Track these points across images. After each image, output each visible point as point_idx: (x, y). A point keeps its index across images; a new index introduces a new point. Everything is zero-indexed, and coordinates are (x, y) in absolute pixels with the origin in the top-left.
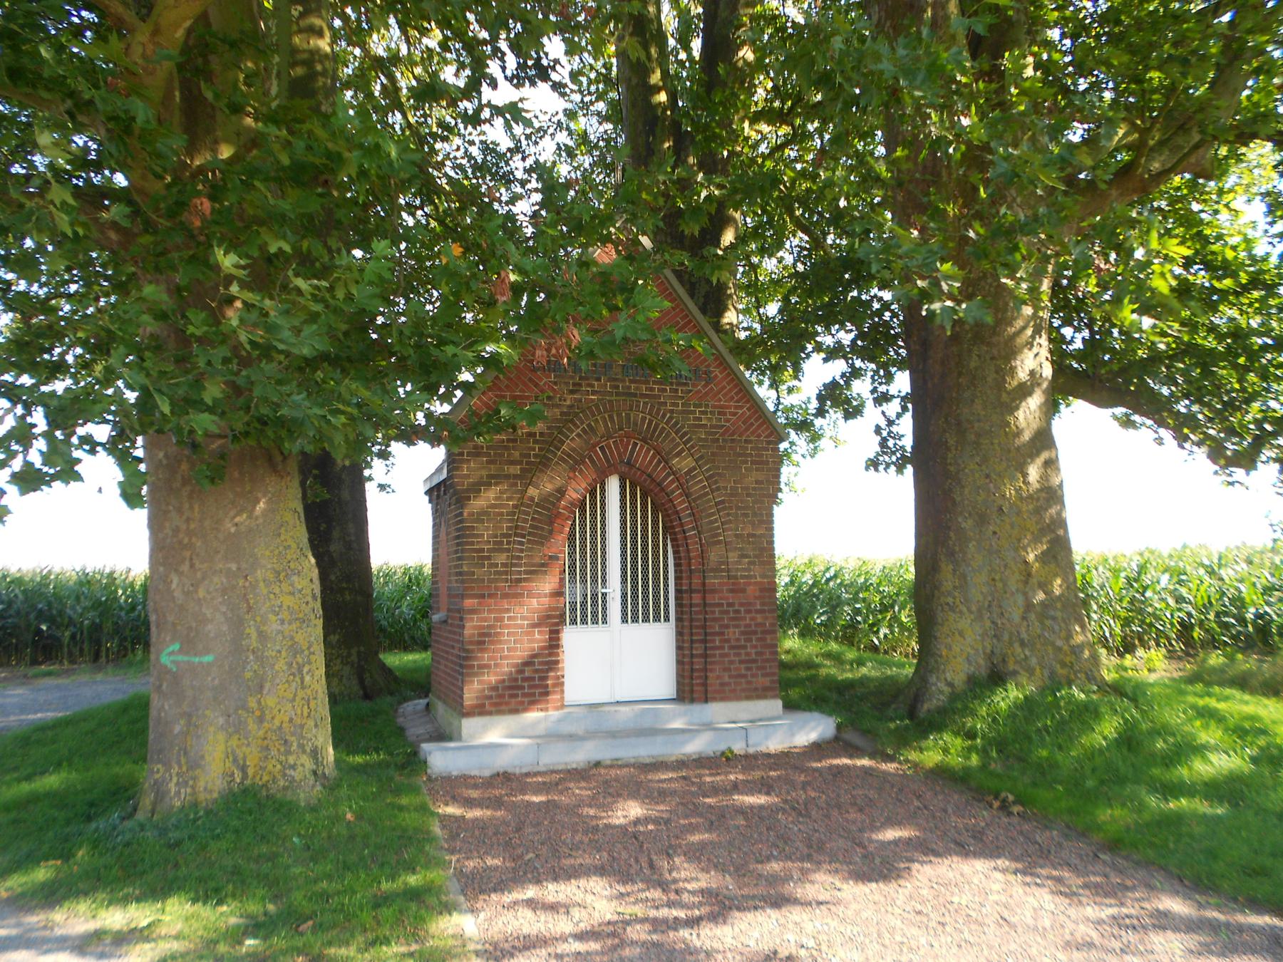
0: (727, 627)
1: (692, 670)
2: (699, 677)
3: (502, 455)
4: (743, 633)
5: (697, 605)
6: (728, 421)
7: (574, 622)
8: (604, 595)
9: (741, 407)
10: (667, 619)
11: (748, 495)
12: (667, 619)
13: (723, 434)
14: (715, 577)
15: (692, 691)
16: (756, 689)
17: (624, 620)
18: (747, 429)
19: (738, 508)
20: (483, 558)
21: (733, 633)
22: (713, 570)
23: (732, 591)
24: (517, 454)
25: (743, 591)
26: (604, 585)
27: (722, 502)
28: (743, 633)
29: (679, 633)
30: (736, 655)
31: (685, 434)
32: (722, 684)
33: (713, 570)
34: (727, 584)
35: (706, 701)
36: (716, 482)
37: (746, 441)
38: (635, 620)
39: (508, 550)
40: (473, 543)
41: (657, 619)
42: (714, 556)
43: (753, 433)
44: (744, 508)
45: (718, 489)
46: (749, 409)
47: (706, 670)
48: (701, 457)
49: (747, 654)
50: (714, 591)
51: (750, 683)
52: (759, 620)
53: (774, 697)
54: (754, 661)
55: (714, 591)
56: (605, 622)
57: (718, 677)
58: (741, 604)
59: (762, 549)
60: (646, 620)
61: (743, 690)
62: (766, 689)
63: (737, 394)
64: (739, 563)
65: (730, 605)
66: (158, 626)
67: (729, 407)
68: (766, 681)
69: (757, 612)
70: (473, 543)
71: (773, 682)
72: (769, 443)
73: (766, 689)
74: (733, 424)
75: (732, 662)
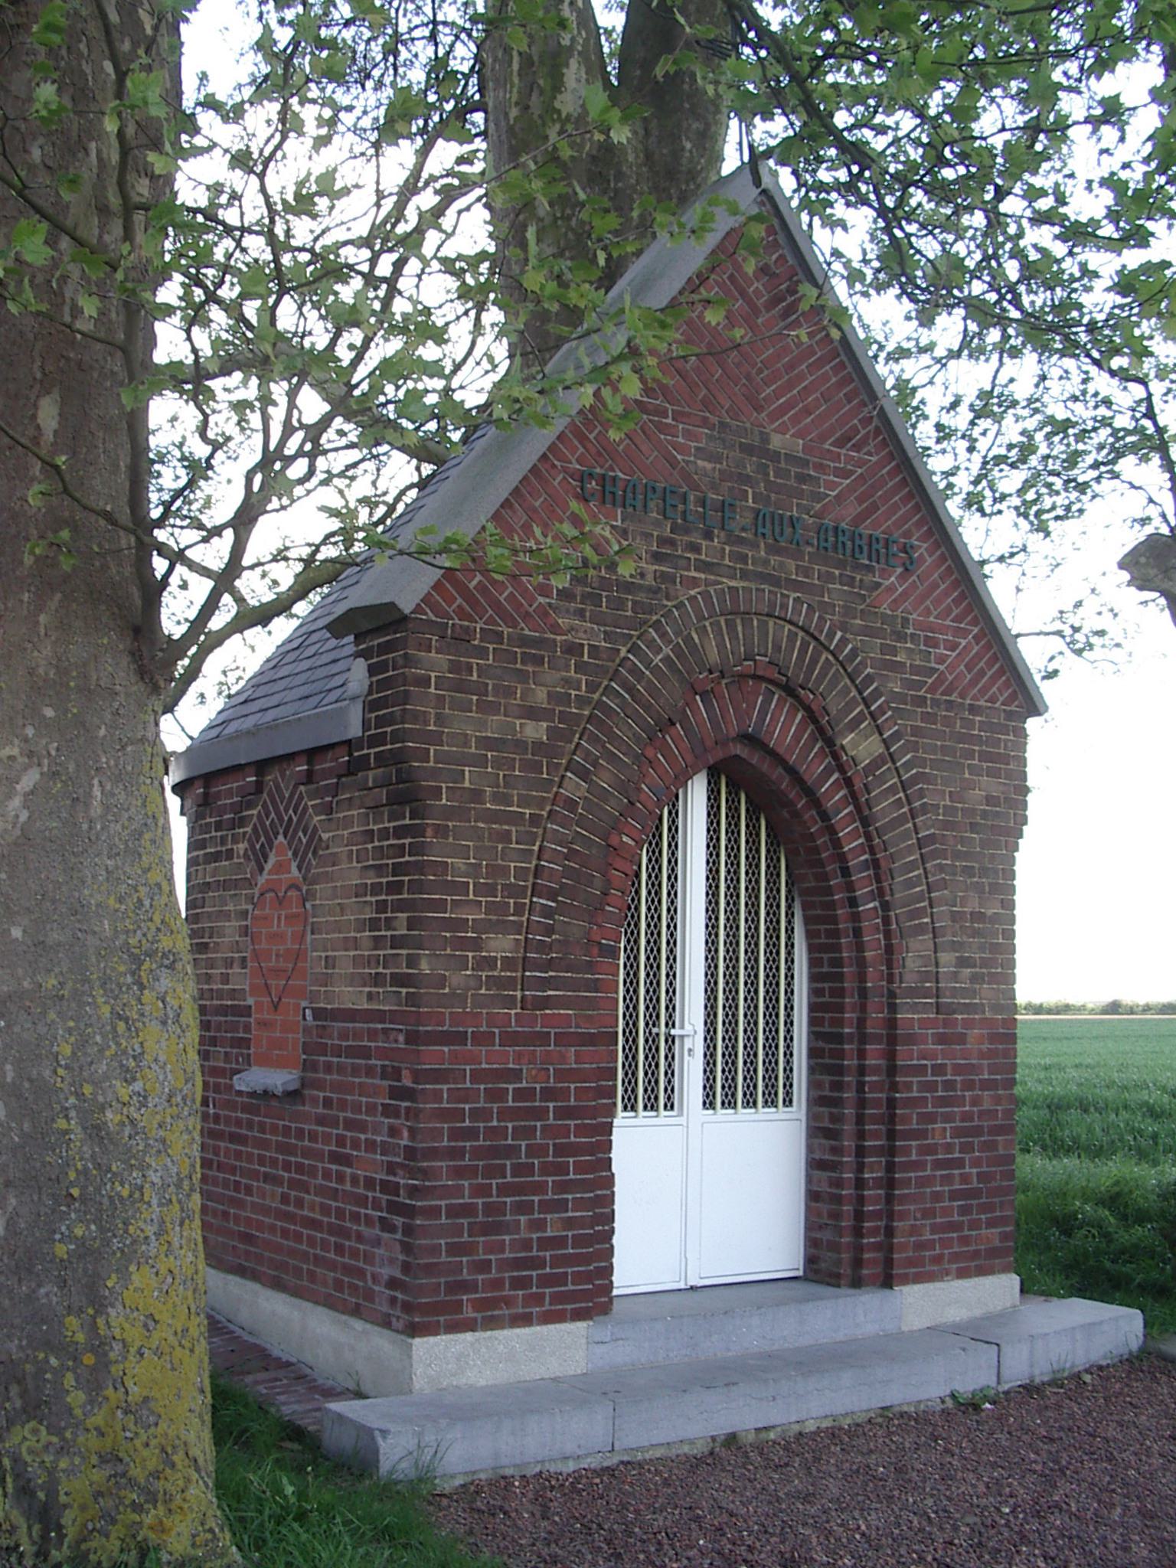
0: (931, 1118)
1: (859, 1216)
2: (875, 1231)
3: (510, 692)
4: (958, 1133)
5: (876, 1070)
6: (941, 660)
7: (630, 1106)
8: (671, 1040)
9: (964, 633)
10: (788, 1102)
11: (973, 827)
12: (788, 1102)
13: (932, 689)
14: (914, 1008)
15: (858, 1263)
16: (976, 1254)
17: (709, 1103)
18: (974, 682)
19: (957, 856)
20: (463, 944)
21: (942, 1133)
22: (913, 992)
23: (941, 1039)
24: (541, 696)
25: (962, 1039)
26: (671, 1023)
27: (932, 839)
28: (958, 1133)
29: (822, 1133)
30: (529, 1169)
31: (869, 679)
32: (920, 1246)
33: (913, 992)
34: (933, 1023)
35: (888, 1281)
36: (921, 794)
37: (973, 709)
38: (729, 1103)
39: (517, 928)
40: (441, 906)
41: (770, 1102)
42: (914, 957)
43: (983, 691)
44: (965, 856)
45: (924, 809)
46: (977, 639)
47: (891, 1216)
48: (897, 736)
49: (965, 1179)
50: (911, 1039)
51: (965, 1240)
52: (986, 1105)
53: (1005, 1270)
54: (974, 1193)
55: (911, 1039)
56: (669, 1106)
57: (914, 1230)
58: (958, 1069)
59: (995, 948)
60: (750, 1103)
61: (955, 1257)
62: (993, 1253)
63: (957, 602)
64: (955, 977)
65: (939, 1070)
66: (490, 1338)
67: (943, 630)
68: (992, 1235)
69: (986, 1085)
70: (441, 906)
71: (1004, 1237)
72: (1010, 715)
73: (993, 1253)
74: (951, 668)
75: (937, 1197)
